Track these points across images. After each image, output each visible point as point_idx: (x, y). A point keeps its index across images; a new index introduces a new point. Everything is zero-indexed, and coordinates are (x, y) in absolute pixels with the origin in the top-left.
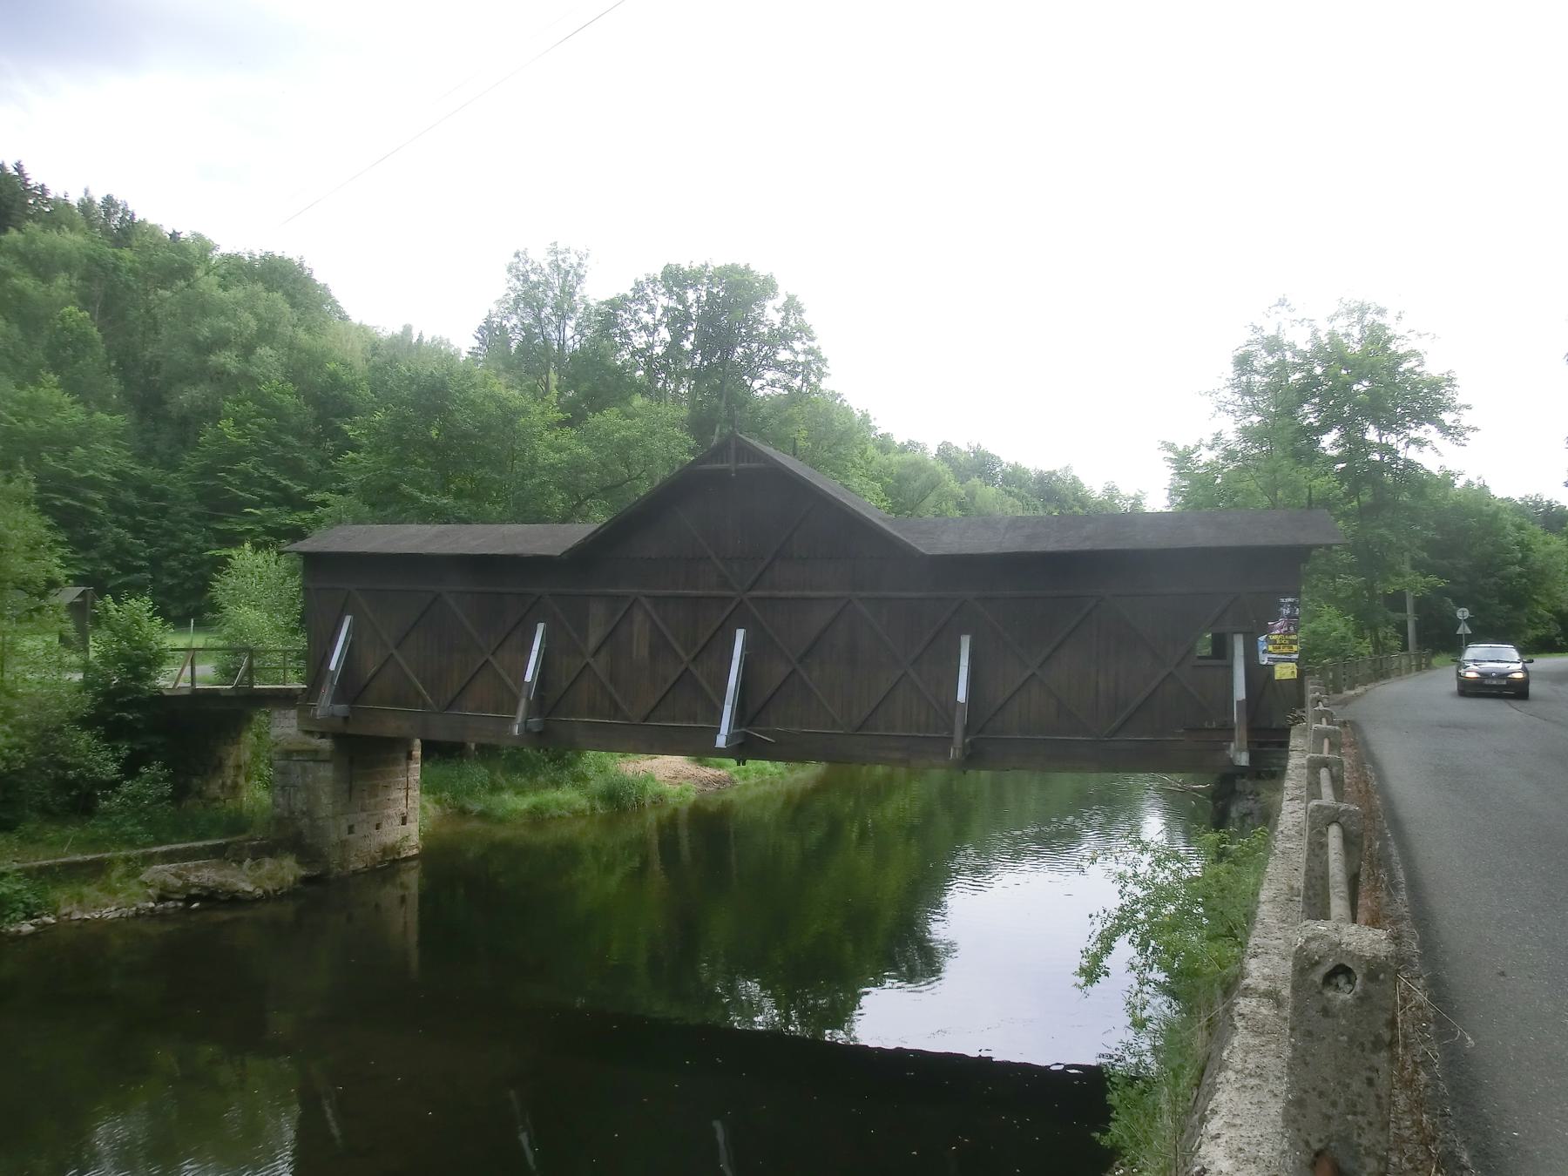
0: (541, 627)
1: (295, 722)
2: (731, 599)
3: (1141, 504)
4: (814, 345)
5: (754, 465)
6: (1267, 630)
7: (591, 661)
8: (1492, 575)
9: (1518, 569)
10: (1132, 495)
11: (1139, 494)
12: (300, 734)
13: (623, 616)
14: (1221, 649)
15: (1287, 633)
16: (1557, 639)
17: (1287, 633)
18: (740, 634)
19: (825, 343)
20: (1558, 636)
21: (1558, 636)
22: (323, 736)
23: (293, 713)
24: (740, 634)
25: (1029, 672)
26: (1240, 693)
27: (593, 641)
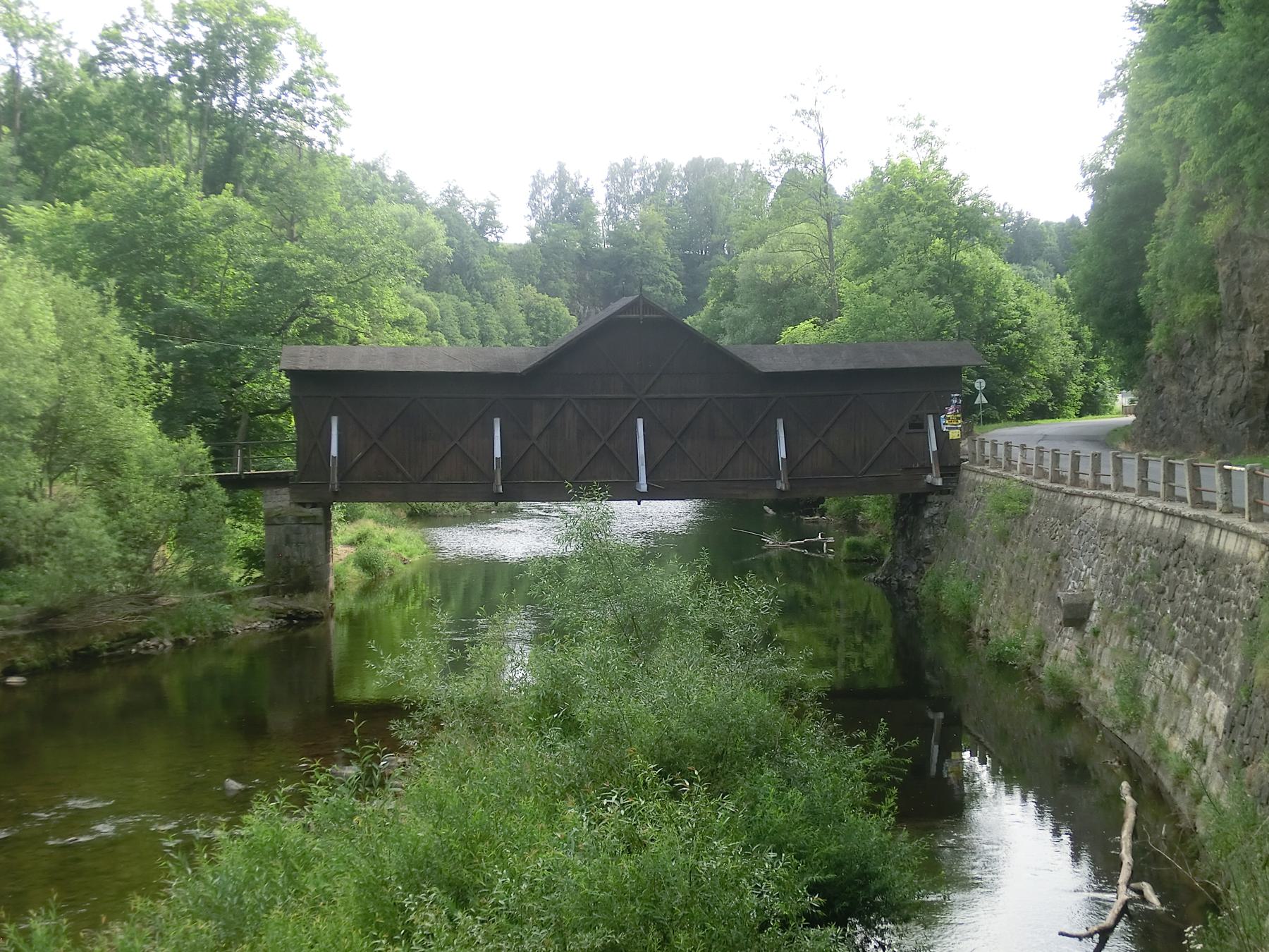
0: (780, 422)
1: (287, 497)
2: (634, 399)
3: (494, 214)
4: (336, 92)
5: (655, 316)
6: (945, 412)
7: (536, 443)
8: (994, 342)
9: (1018, 335)
10: (482, 201)
11: (492, 199)
12: (293, 506)
13: (836, 421)
14: (920, 426)
15: (955, 413)
16: (1049, 404)
17: (955, 413)
18: (640, 422)
19: (347, 89)
20: (1050, 401)
21: (1050, 401)
22: (314, 505)
23: (285, 490)
24: (640, 422)
25: (816, 440)
26: (933, 447)
27: (536, 431)
